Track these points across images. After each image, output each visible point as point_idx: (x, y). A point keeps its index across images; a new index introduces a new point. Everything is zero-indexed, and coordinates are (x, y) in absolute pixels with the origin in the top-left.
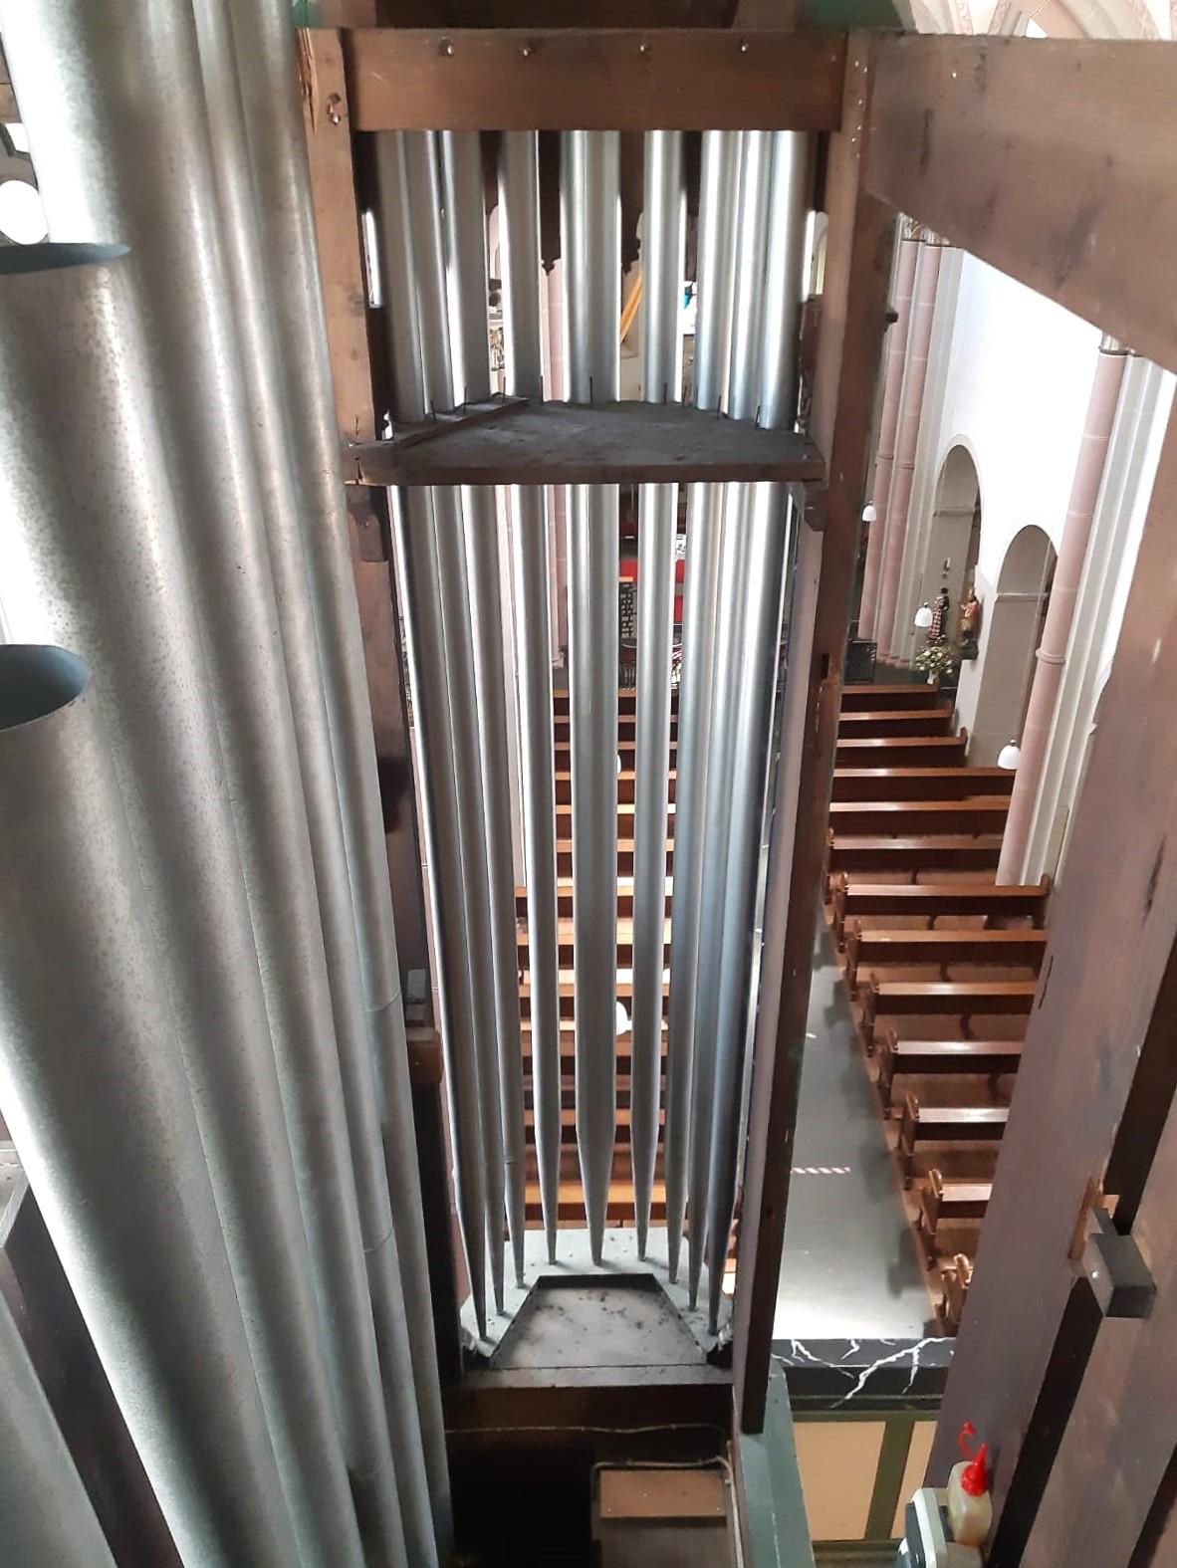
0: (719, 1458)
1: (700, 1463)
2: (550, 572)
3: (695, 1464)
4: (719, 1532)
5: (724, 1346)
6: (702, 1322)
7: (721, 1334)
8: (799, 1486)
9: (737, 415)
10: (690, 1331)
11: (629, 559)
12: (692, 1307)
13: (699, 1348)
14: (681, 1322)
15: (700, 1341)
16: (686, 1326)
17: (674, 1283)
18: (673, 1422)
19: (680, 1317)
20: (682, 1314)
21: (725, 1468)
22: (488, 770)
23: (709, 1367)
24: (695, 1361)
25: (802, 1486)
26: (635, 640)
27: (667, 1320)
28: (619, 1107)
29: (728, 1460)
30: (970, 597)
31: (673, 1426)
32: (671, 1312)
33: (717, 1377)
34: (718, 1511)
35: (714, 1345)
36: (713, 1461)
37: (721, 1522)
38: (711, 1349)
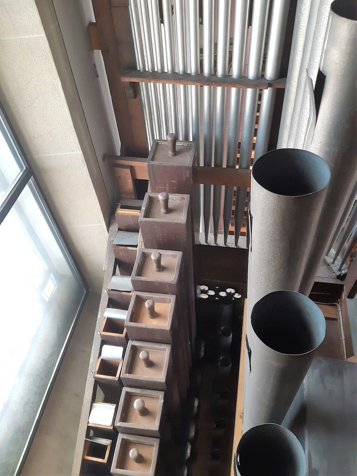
0: (336, 303)
1: (329, 304)
2: (145, 54)
3: (328, 304)
4: (335, 322)
5: (344, 275)
6: (336, 267)
7: (343, 271)
8: (251, 319)
9: (160, 72)
10: (332, 269)
11: (201, 55)
12: (333, 263)
13: (334, 274)
14: (329, 266)
15: (335, 272)
16: (330, 267)
17: (327, 256)
18: (322, 292)
19: (328, 265)
20: (329, 264)
21: (337, 306)
22: (110, 119)
23: (337, 280)
24: (333, 277)
25: (251, 319)
26: (264, 58)
27: (324, 265)
28: (232, 215)
29: (338, 304)
30: (129, 185)
31: (322, 293)
32: (325, 263)
33: (339, 282)
34: (334, 317)
35: (340, 274)
36: (334, 304)
37: (336, 319)
38: (338, 275)
